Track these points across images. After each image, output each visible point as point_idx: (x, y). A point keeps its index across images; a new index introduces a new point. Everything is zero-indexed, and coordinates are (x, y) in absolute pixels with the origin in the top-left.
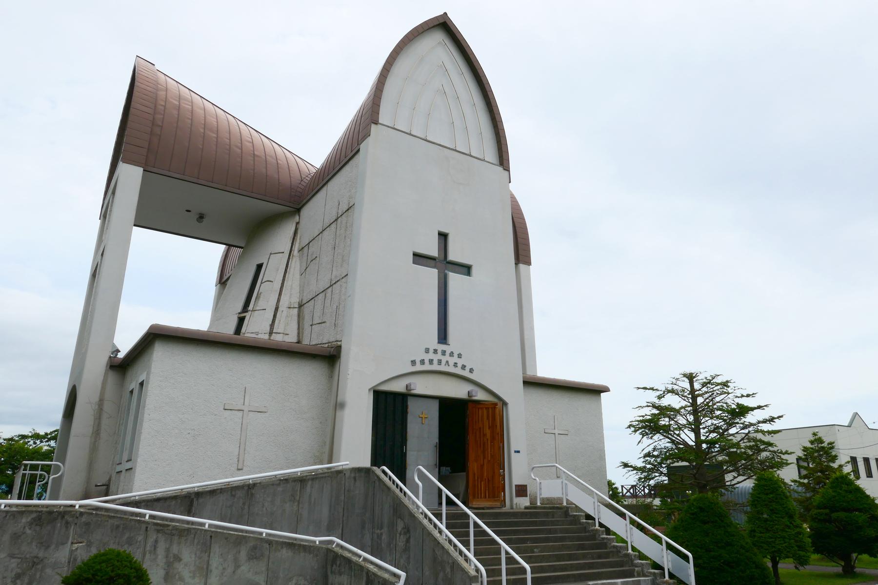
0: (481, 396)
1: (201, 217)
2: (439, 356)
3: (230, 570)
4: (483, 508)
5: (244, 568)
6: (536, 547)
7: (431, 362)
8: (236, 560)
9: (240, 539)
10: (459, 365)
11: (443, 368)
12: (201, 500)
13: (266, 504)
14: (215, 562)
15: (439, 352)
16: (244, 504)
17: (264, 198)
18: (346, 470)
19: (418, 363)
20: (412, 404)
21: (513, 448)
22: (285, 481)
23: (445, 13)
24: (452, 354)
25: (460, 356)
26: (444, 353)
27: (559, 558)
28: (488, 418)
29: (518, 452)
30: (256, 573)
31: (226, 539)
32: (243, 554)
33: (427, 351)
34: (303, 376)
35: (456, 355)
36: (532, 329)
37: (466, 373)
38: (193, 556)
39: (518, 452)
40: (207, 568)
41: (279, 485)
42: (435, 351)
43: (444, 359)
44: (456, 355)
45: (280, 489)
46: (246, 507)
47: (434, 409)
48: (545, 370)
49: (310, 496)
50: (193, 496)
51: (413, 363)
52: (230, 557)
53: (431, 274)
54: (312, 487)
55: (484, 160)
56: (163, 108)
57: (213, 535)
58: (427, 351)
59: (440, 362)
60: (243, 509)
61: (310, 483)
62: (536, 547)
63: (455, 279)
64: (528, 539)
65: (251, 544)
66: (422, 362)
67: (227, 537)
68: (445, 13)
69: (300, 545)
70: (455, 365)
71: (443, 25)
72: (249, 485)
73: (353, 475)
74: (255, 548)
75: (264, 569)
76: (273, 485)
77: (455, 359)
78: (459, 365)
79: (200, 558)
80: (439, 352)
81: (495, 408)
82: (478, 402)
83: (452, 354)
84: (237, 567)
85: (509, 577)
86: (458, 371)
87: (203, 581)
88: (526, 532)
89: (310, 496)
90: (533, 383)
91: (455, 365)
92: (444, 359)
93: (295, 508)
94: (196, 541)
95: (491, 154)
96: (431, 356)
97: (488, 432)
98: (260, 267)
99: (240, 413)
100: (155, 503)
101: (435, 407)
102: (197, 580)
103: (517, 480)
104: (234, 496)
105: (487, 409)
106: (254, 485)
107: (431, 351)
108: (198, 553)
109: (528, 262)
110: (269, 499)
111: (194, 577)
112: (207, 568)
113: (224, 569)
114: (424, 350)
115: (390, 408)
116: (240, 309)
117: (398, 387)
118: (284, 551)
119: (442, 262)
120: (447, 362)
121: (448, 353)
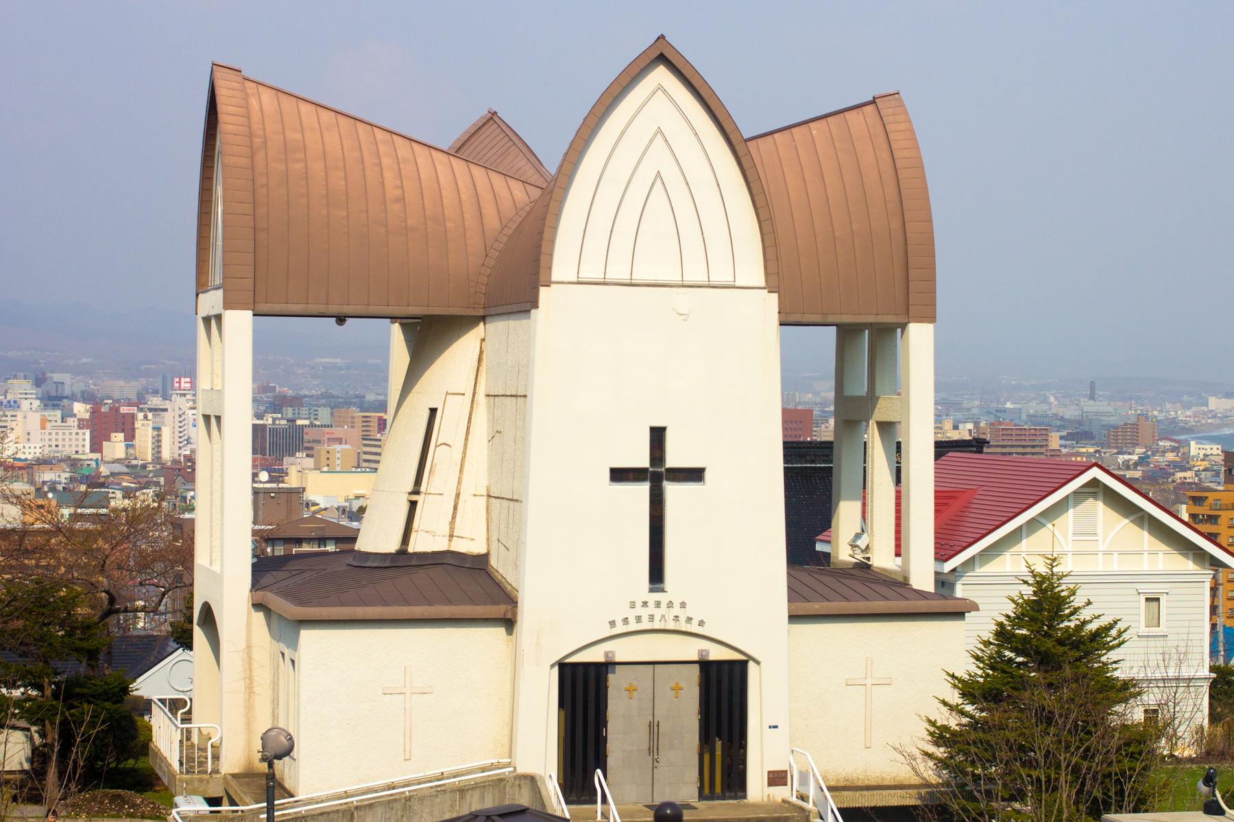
2: (651, 609)
10: (683, 619)
15: (651, 604)
17: (524, 149)
19: (619, 623)
20: (615, 681)
24: (670, 604)
25: (683, 605)
26: (658, 604)
29: (776, 727)
33: (633, 605)
34: (492, 127)
35: (677, 605)
39: (776, 727)
42: (645, 604)
43: (658, 613)
44: (677, 605)
51: (612, 623)
63: (673, 491)
78: (683, 619)
80: (651, 604)
92: (658, 613)
96: (639, 611)
98: (433, 411)
99: (401, 697)
107: (639, 604)
115: (583, 692)
116: (410, 488)
117: (595, 655)
119: (657, 473)
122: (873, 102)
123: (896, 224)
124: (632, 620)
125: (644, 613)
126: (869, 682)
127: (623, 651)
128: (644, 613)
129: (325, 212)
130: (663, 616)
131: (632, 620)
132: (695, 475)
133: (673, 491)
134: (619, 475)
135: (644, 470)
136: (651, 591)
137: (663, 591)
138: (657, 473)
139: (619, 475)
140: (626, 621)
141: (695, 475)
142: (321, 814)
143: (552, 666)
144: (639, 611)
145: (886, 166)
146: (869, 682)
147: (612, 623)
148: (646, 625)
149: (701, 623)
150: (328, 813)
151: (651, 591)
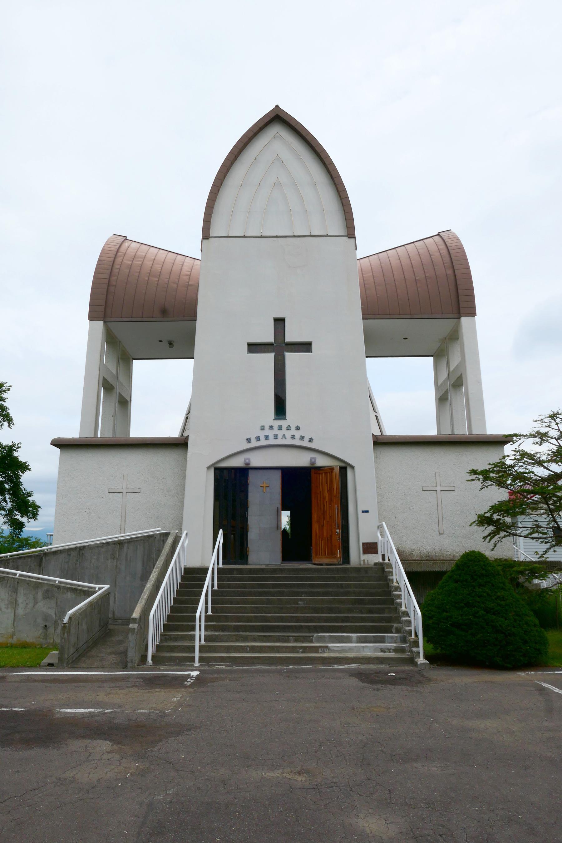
0: (322, 462)
1: (171, 343)
3: (31, 605)
4: (321, 565)
5: (40, 604)
6: (301, 600)
7: (267, 437)
8: (35, 598)
9: (38, 585)
11: (280, 441)
12: (47, 558)
13: (93, 561)
14: (21, 599)
15: (276, 428)
16: (77, 561)
18: (157, 534)
19: (253, 440)
20: (252, 477)
21: (361, 508)
22: (114, 543)
23: (277, 106)
24: (289, 428)
26: (280, 428)
27: (316, 610)
28: (327, 483)
29: (367, 512)
30: (49, 608)
31: (28, 584)
32: (40, 595)
33: (263, 428)
35: (293, 428)
36: (479, 382)
37: (305, 443)
38: (7, 595)
39: (367, 512)
40: (16, 603)
41: (102, 547)
42: (271, 427)
43: (280, 434)
44: (293, 428)
45: (103, 550)
46: (78, 563)
47: (276, 480)
48: (392, 429)
49: (127, 554)
50: (42, 556)
51: (249, 440)
52: (31, 596)
53: (267, 360)
54: (128, 548)
55: (327, 236)
56: (117, 271)
57: (19, 581)
58: (263, 428)
59: (276, 437)
60: (76, 564)
61: (126, 545)
62: (301, 600)
63: (291, 358)
64: (302, 593)
65: (46, 588)
66: (258, 439)
67: (29, 583)
68: (277, 106)
69: (81, 590)
70: (293, 437)
71: (277, 118)
72: (80, 548)
73: (162, 538)
74: (47, 591)
75: (54, 605)
76: (98, 547)
77: (293, 432)
79: (11, 596)
80: (276, 428)
81: (332, 472)
82: (319, 468)
83: (289, 428)
84: (36, 603)
85: (193, 623)
86: (297, 442)
87: (13, 611)
88: (299, 586)
89: (127, 554)
90: (381, 443)
91: (293, 437)
92: (280, 434)
93: (115, 563)
94: (8, 585)
95: (336, 226)
96: (267, 432)
97: (327, 495)
99: (120, 495)
100: (19, 560)
101: (277, 478)
102: (9, 610)
103: (365, 538)
104: (70, 555)
105: (326, 473)
106: (84, 547)
107: (267, 427)
108: (10, 593)
109: (472, 312)
110: (95, 557)
111: (7, 608)
112: (16, 603)
113: (27, 604)
114: (259, 428)
117: (237, 462)
118: (69, 593)
119: (280, 346)
120: (284, 435)
121: (284, 428)
122: (438, 235)
123: (450, 272)
124: (262, 438)
125: (271, 434)
126: (439, 488)
127: (258, 460)
128: (271, 434)
129: (147, 279)
130: (284, 435)
131: (262, 438)
132: (305, 347)
133: (291, 358)
134: (253, 347)
135: (270, 344)
136: (276, 419)
137: (285, 419)
138: (280, 346)
139: (253, 347)
140: (258, 439)
141: (305, 347)
142: (20, 558)
143: (208, 468)
144: (267, 432)
145: (452, 278)
146: (439, 488)
147: (249, 440)
148: (271, 441)
149: (311, 440)
150: (25, 557)
151: (276, 419)
